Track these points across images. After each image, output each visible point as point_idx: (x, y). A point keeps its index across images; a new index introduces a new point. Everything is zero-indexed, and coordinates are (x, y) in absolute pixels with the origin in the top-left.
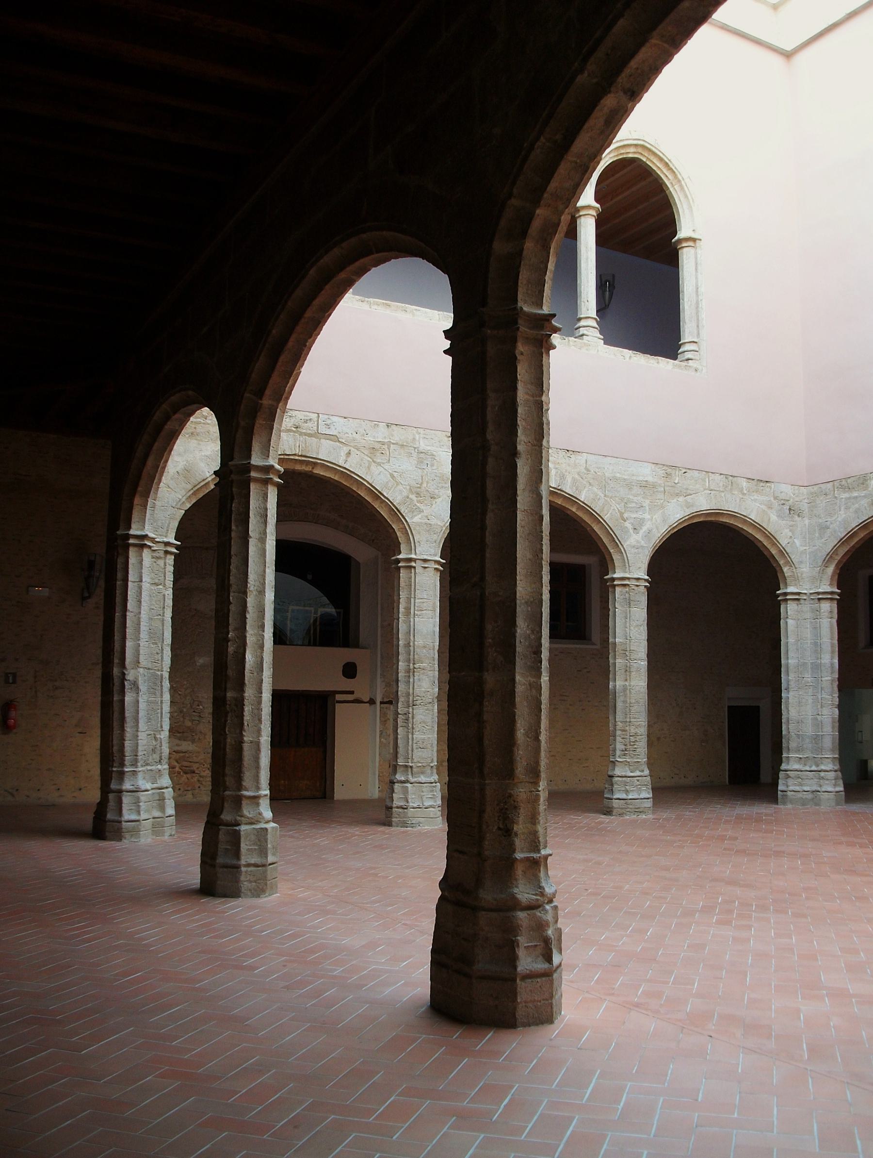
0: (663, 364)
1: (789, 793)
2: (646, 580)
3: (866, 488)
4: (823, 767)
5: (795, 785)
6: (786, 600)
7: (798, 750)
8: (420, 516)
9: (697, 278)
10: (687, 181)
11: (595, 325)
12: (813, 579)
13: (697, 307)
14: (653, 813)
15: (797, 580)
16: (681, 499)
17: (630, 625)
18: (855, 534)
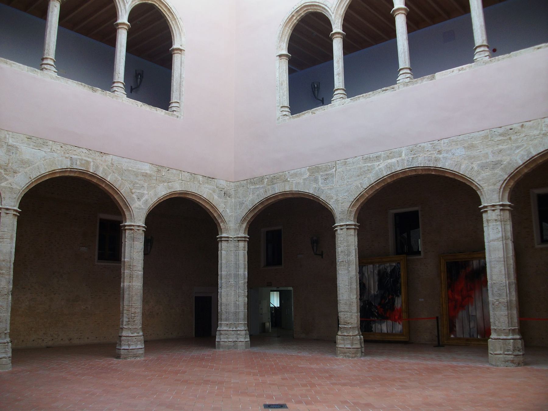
0: (160, 112)
1: (221, 343)
2: (143, 227)
3: (263, 184)
4: (239, 329)
5: (225, 338)
6: (221, 241)
7: (226, 320)
8: (6, 183)
9: (181, 70)
10: (179, 20)
11: (122, 86)
12: (236, 230)
13: (180, 85)
14: (145, 356)
15: (227, 230)
16: (165, 184)
17: (134, 251)
18: (257, 207)
